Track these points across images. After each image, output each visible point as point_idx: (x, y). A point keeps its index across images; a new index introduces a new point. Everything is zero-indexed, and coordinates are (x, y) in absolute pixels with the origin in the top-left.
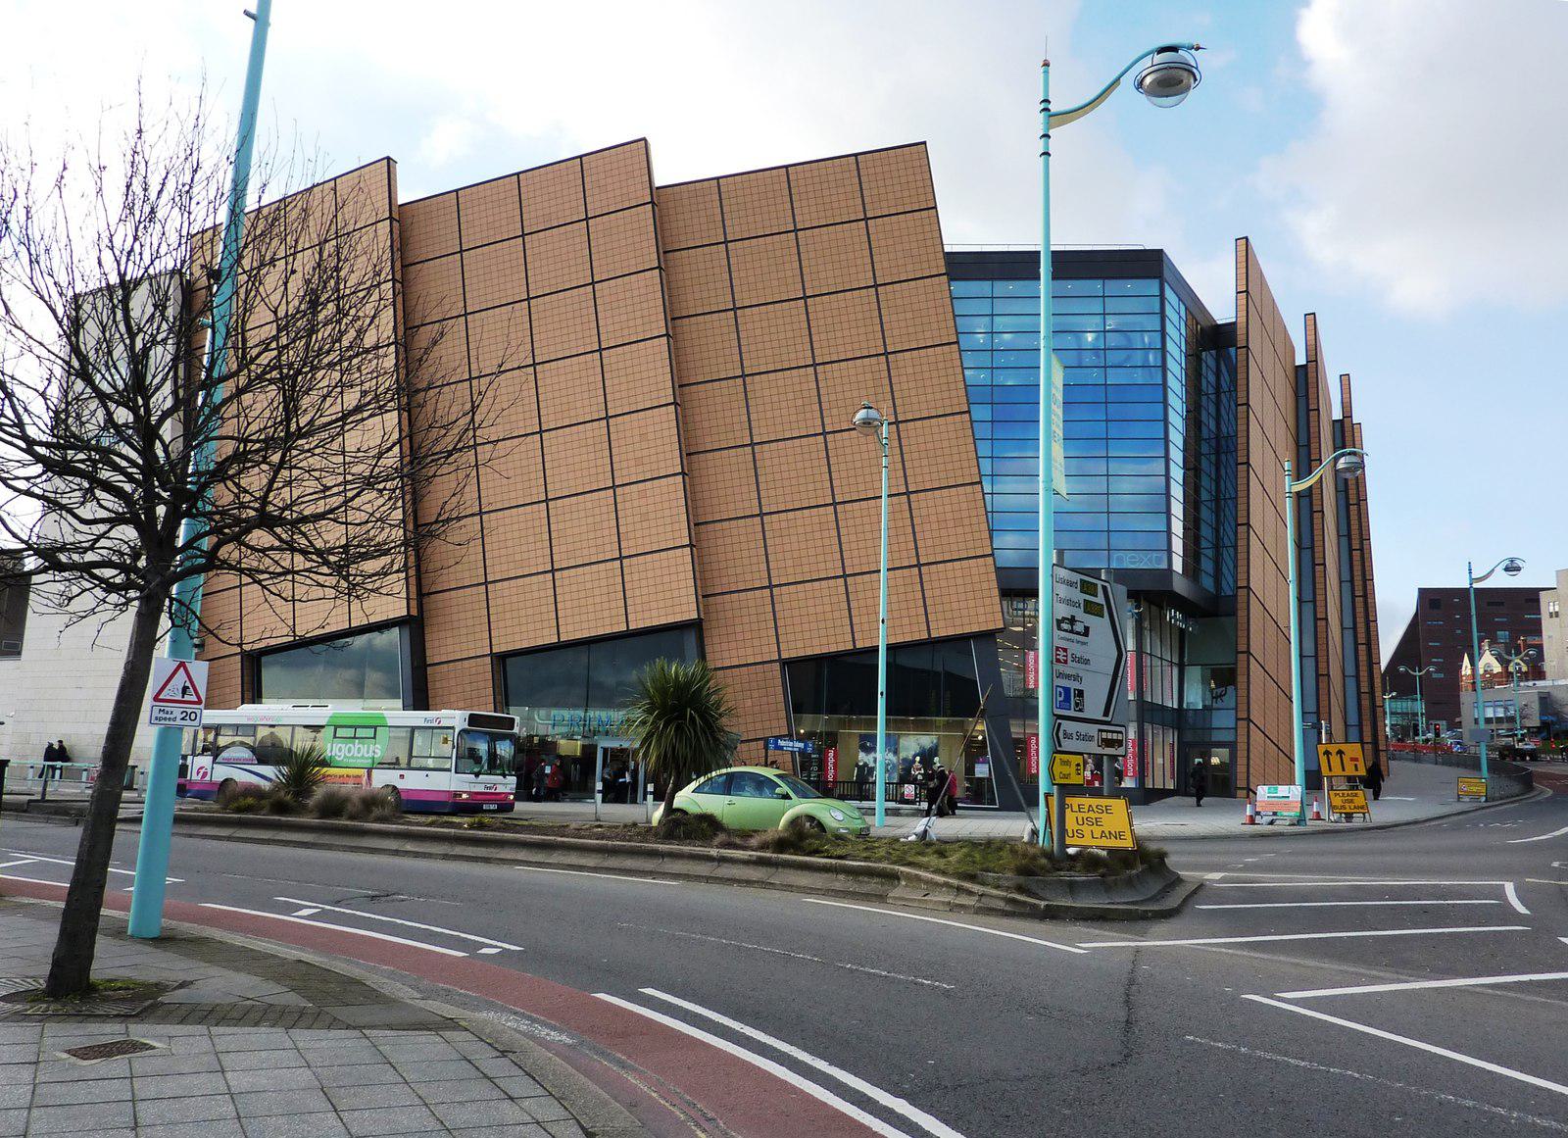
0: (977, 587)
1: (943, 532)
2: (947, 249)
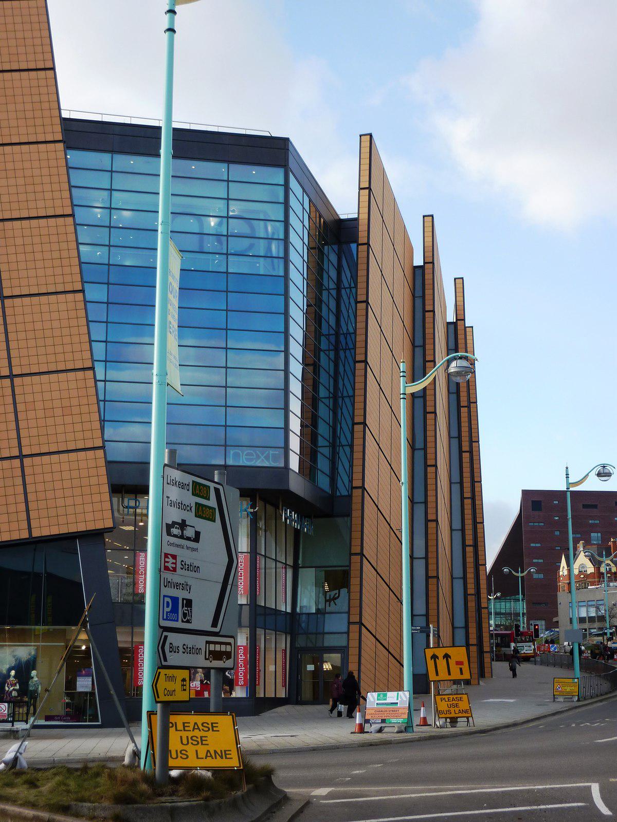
0: (85, 482)
1: (50, 421)
2: (65, 115)
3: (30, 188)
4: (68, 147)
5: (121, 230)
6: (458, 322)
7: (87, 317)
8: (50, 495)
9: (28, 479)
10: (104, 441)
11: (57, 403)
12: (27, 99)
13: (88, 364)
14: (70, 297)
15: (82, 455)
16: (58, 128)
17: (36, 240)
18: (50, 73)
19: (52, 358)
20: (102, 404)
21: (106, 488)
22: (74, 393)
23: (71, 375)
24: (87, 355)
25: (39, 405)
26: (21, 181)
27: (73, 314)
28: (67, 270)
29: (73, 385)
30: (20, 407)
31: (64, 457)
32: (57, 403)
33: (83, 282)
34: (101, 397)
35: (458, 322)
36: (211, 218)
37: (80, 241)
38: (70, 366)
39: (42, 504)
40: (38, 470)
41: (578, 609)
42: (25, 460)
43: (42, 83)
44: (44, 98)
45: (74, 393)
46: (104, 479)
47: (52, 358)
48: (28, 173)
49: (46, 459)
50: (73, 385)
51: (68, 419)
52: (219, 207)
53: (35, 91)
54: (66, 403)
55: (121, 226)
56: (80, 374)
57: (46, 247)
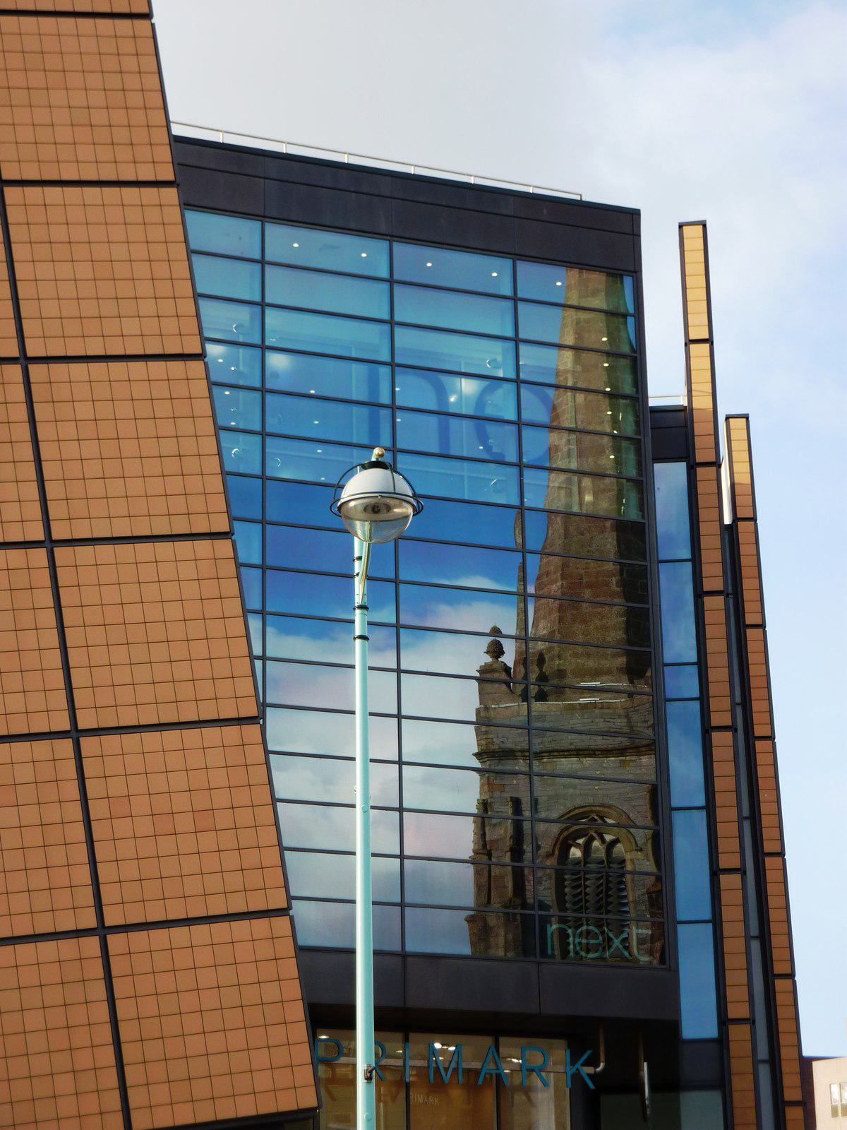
1: (166, 845)
2: (177, 130)
3: (106, 289)
4: (187, 204)
5: (313, 403)
6: (740, 524)
7: (264, 742)
8: (171, 1026)
9: (120, 988)
10: (290, 898)
11: (181, 802)
12: (94, 80)
13: (253, 712)
14: (203, 546)
15: (241, 927)
16: (165, 153)
17: (124, 410)
18: (141, 24)
19: (178, 504)
20: (258, 664)
21: (297, 1012)
22: (219, 778)
23: (211, 733)
24: (246, 687)
25: (140, 805)
26: (84, 271)
27: (210, 588)
28: (194, 484)
29: (215, 757)
30: (96, 809)
31: (200, 931)
32: (181, 802)
33: (232, 519)
34: (257, 651)
35: (740, 524)
36: (464, 380)
37: (270, 748)
38: (208, 713)
39: (154, 1050)
40: (142, 964)
41: (665, 704)
42: (113, 940)
43: (127, 46)
44: (132, 81)
45: (219, 778)
46: (294, 989)
47: (178, 504)
48: (101, 252)
49: (159, 936)
50: (215, 757)
51: (207, 841)
52: (494, 358)
53: (110, 63)
54: (201, 802)
55: (312, 392)
56: (231, 732)
57: (146, 428)
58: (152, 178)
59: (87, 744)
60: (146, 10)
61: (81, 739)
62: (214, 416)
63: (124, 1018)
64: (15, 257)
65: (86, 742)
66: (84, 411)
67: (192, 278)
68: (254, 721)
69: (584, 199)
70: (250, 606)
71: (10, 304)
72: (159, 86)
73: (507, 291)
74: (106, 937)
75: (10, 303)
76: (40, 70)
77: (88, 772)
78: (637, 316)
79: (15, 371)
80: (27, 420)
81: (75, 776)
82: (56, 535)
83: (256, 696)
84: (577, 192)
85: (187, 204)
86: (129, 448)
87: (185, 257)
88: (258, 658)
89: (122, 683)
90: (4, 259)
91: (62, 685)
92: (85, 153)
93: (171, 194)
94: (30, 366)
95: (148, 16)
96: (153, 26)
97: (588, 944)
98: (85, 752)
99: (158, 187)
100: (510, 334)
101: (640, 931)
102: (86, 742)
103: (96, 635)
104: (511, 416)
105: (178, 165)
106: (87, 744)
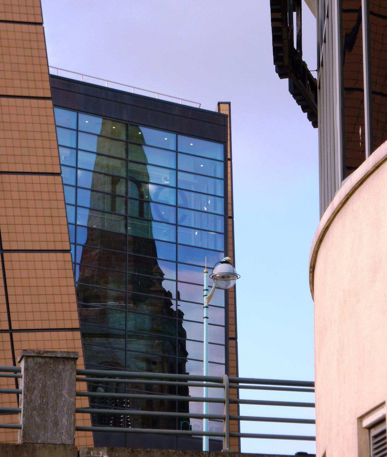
2: (52, 72)
4: (55, 105)
18: (38, 27)
58: (61, 249)
59: (15, 335)
60: (41, 21)
61: (4, 253)
62: (65, 200)
63: (8, 277)
64: (6, 268)
65: (15, 335)
66: (15, 195)
67: (57, 140)
68: (69, 252)
69: (202, 107)
70: (69, 221)
71: (4, 297)
72: (70, 248)
73: (173, 148)
74: (17, 379)
75: (4, 288)
76: (17, 191)
77: (12, 318)
78: (225, 197)
79: (7, 336)
80: (11, 349)
81: (10, 340)
82: (13, 327)
83: (72, 261)
84: (199, 102)
85: (55, 105)
86: (32, 212)
87: (57, 147)
88: (73, 244)
89: (29, 320)
90: (1, 269)
91: (10, 340)
92: (17, 83)
93: (50, 103)
94: (13, 334)
95: (41, 24)
96: (43, 27)
97: (162, 178)
98: (14, 339)
99: (45, 100)
100: (174, 167)
101: (216, 426)
102: (15, 335)
103: (19, 291)
104: (173, 203)
105: (53, 88)
106: (15, 335)
